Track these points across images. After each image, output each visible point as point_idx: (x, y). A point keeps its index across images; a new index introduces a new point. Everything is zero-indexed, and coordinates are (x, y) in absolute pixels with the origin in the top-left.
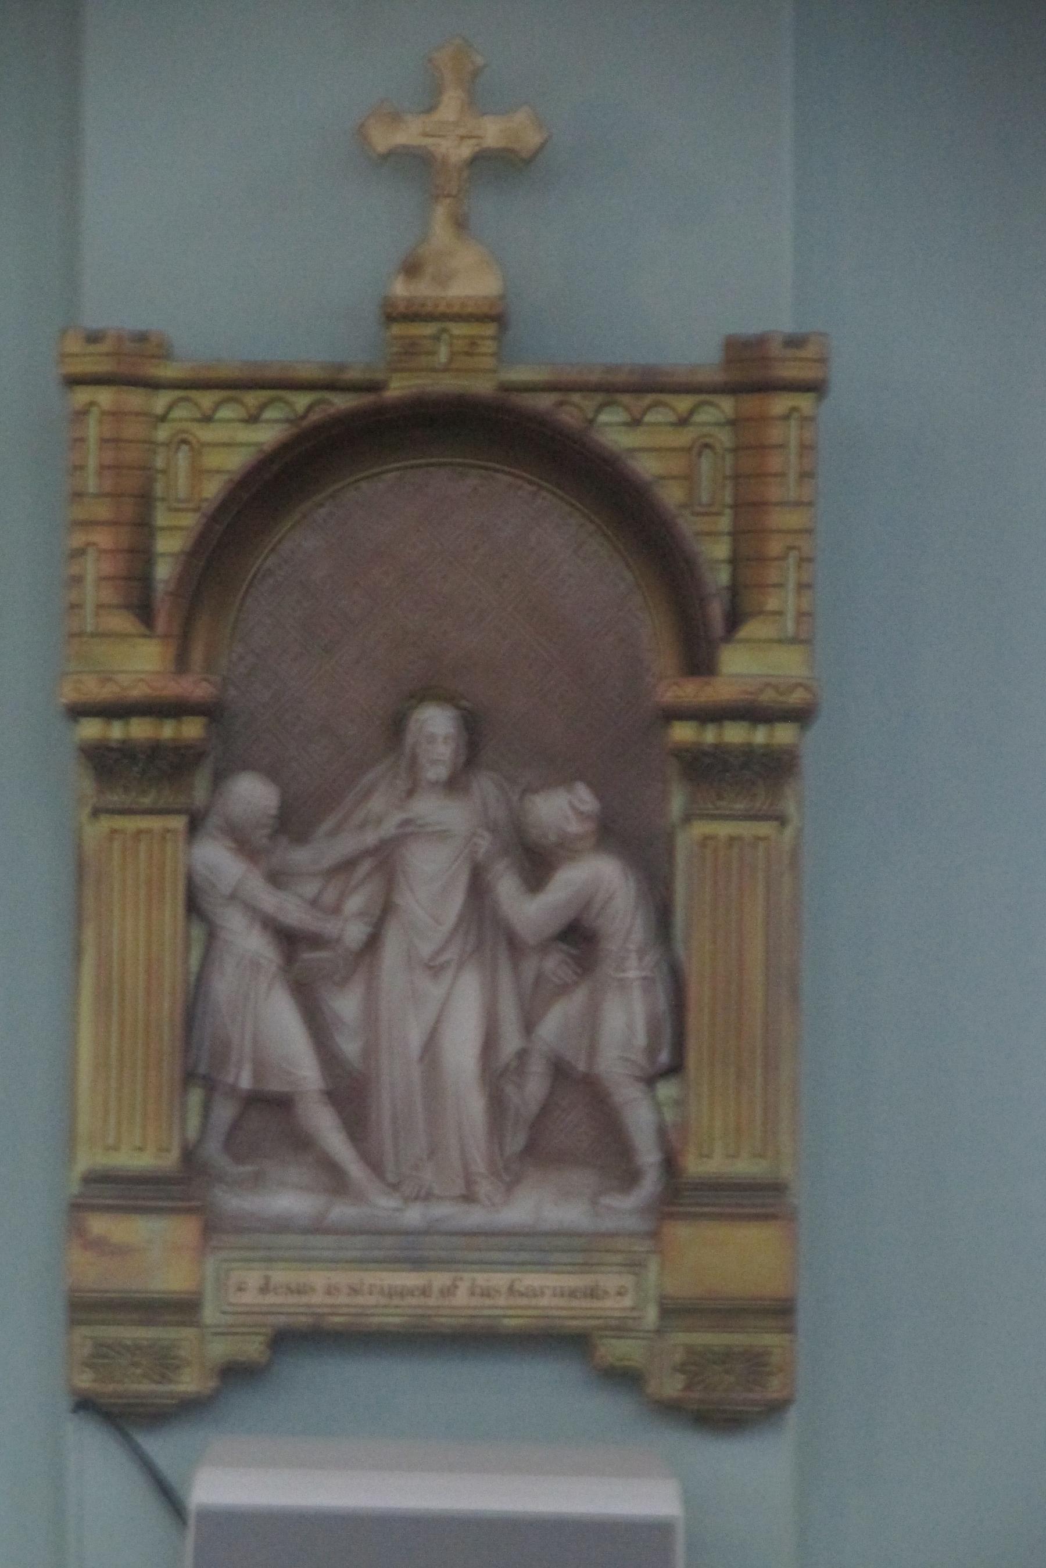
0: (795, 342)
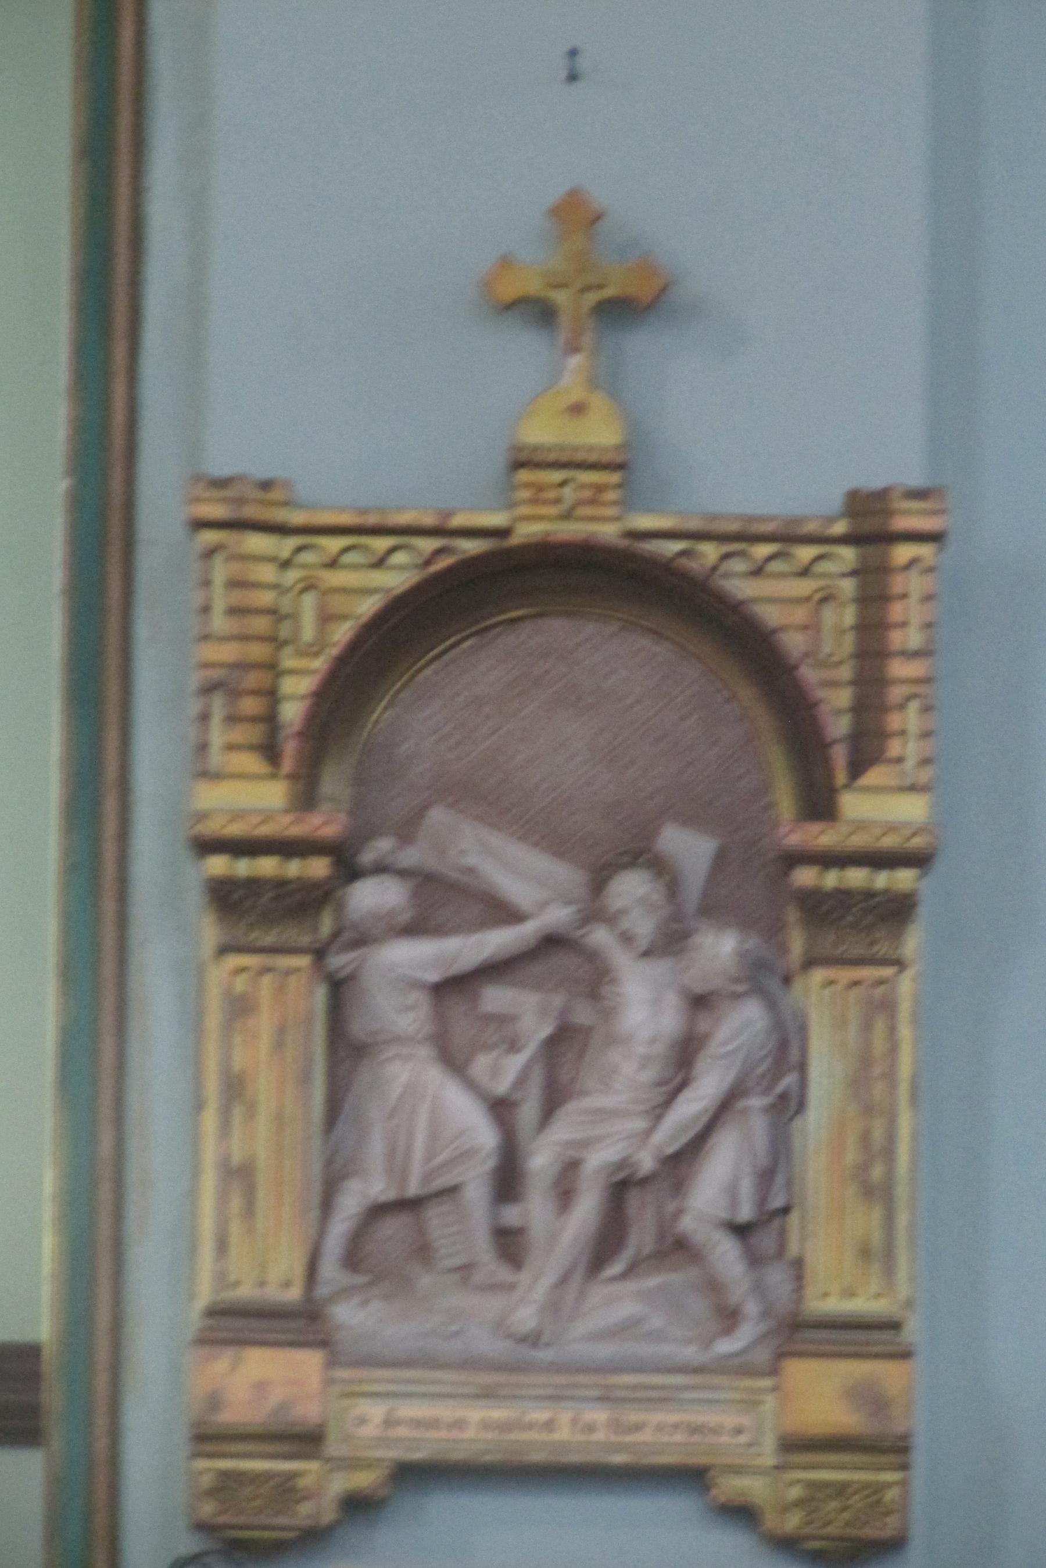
0: (919, 494)
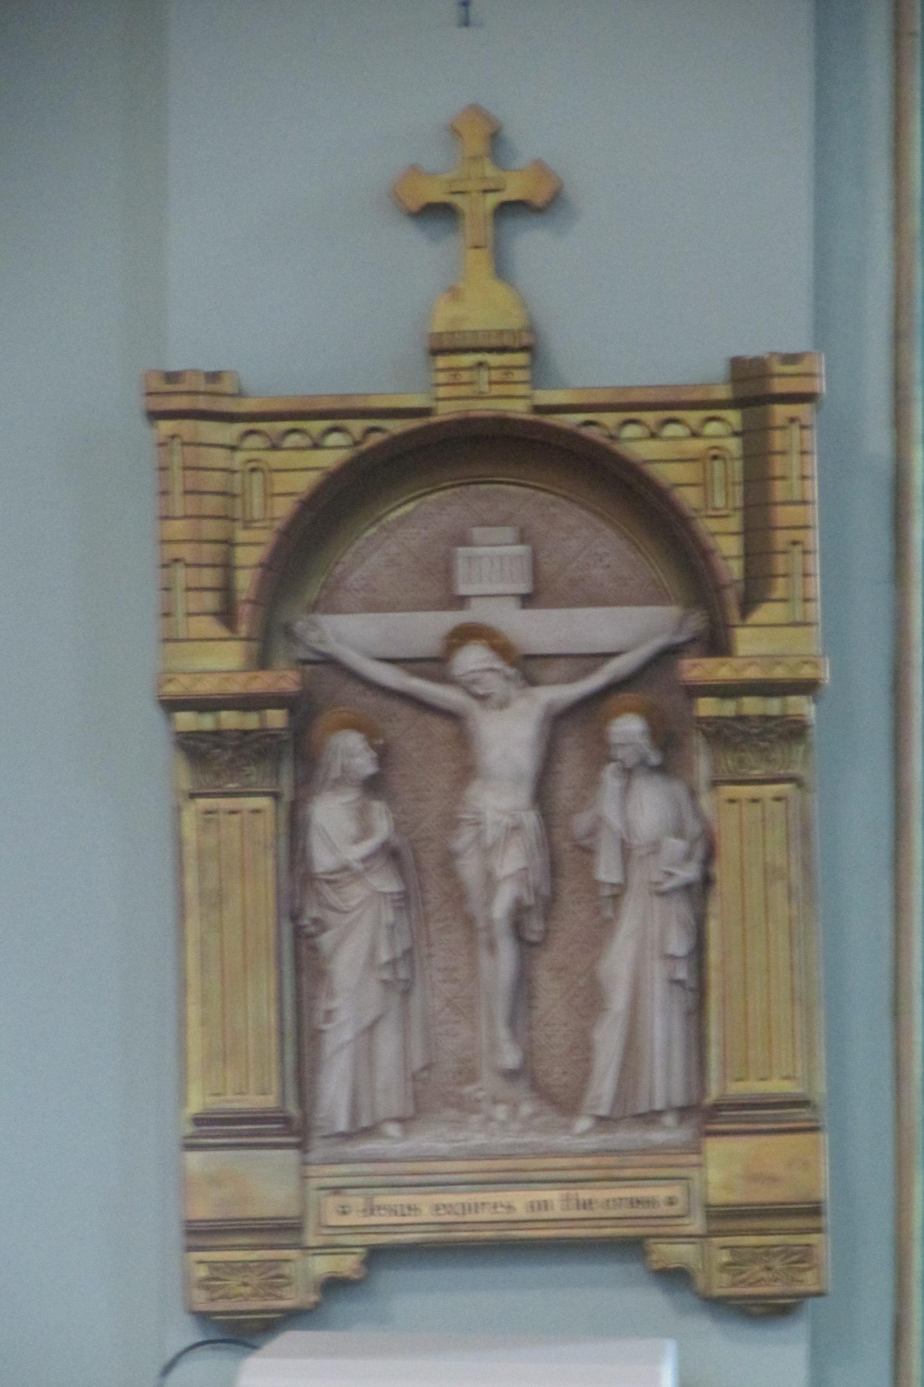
0: (792, 359)
